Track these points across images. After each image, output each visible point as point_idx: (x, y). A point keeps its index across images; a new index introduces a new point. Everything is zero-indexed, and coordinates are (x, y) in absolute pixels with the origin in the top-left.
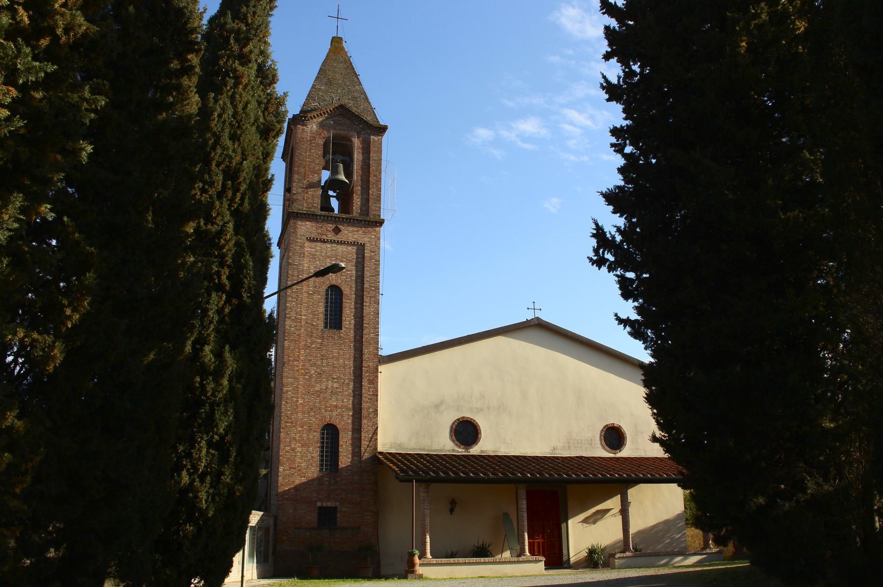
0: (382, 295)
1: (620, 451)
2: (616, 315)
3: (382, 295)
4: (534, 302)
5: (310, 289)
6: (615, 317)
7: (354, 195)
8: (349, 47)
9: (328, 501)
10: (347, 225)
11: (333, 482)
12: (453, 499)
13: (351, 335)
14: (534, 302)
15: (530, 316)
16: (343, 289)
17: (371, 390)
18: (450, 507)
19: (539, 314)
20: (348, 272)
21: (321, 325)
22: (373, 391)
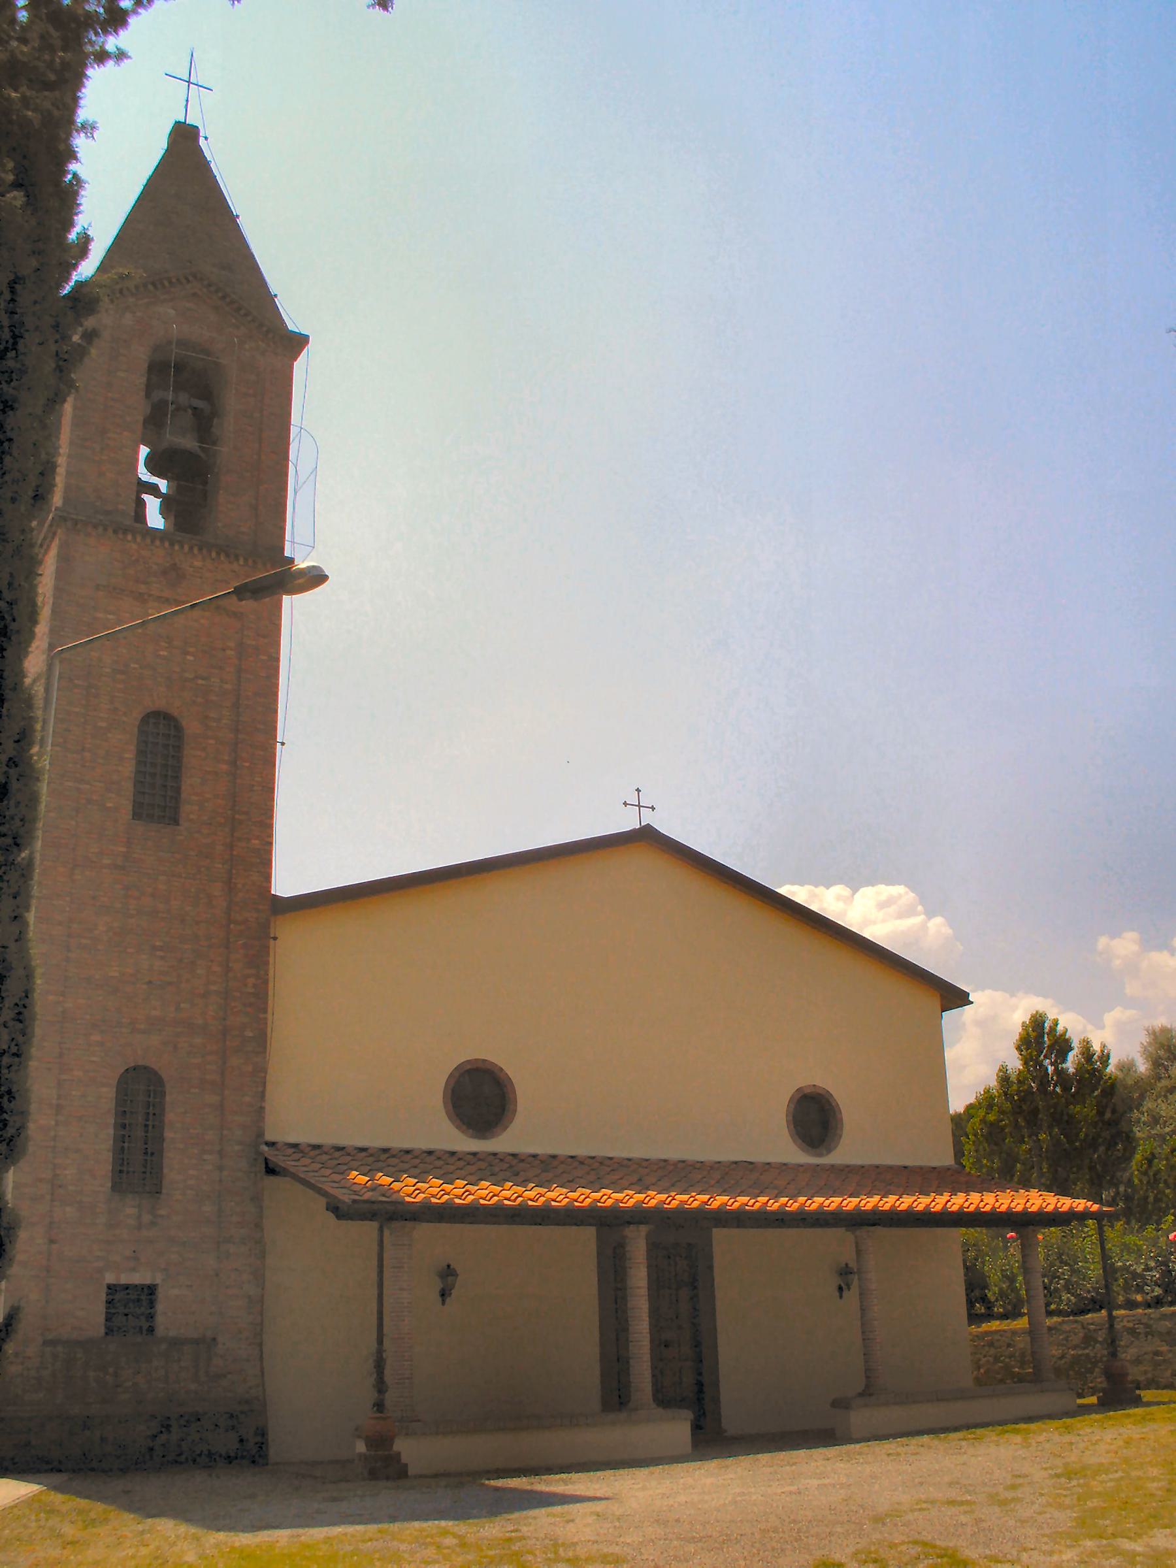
0: (283, 744)
1: (829, 1151)
2: (368, 7)
3: (283, 744)
4: (638, 790)
5: (102, 715)
6: (371, 8)
7: (221, 492)
8: (213, 148)
9: (134, 1269)
10: (958, 1553)
11: (146, 1218)
12: (449, 1266)
13: (645, 1331)
14: (638, 790)
15: (627, 822)
16: (184, 723)
17: (251, 981)
18: (442, 1286)
19: (648, 818)
20: (200, 682)
21: (127, 806)
22: (254, 986)
